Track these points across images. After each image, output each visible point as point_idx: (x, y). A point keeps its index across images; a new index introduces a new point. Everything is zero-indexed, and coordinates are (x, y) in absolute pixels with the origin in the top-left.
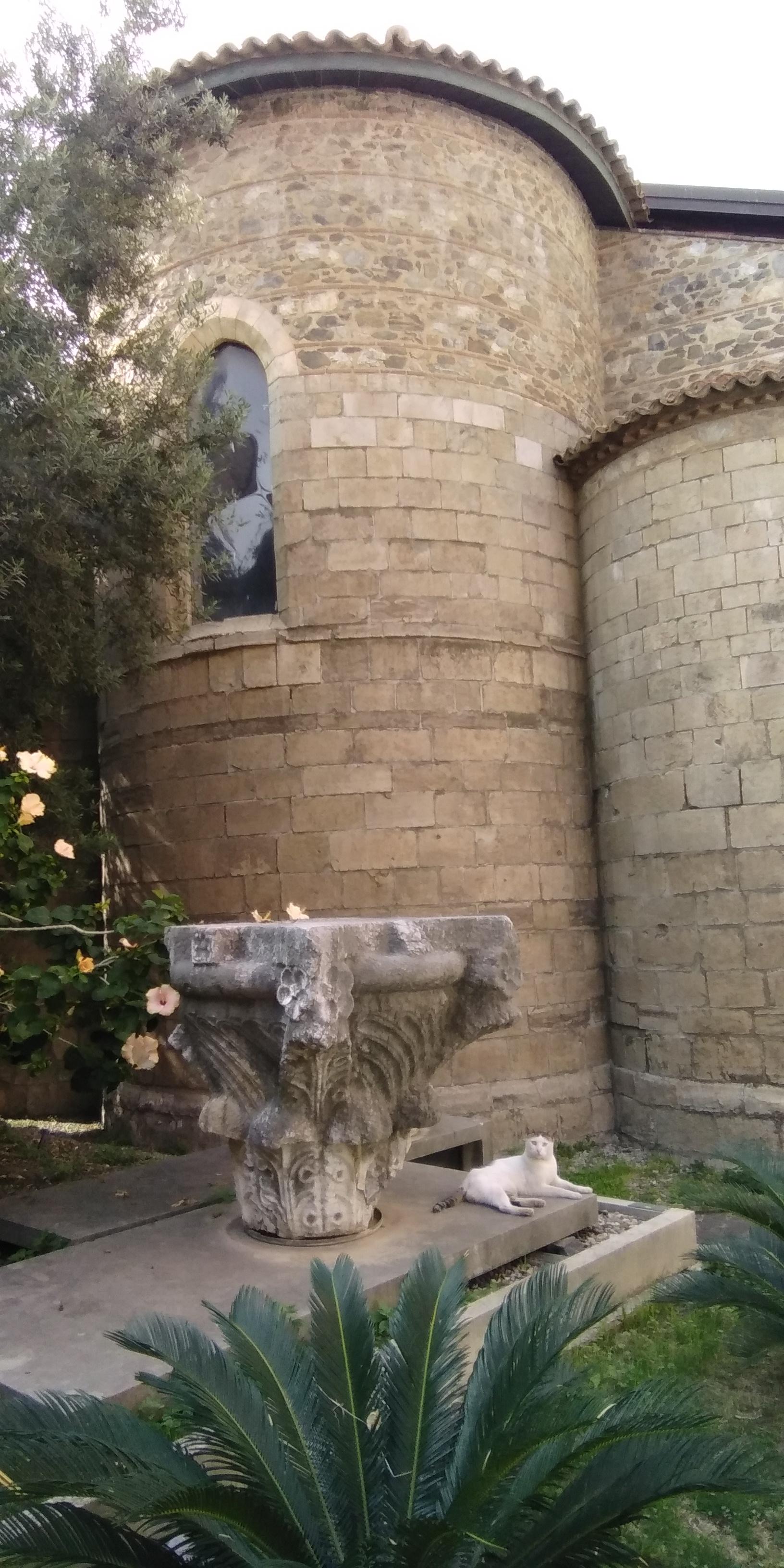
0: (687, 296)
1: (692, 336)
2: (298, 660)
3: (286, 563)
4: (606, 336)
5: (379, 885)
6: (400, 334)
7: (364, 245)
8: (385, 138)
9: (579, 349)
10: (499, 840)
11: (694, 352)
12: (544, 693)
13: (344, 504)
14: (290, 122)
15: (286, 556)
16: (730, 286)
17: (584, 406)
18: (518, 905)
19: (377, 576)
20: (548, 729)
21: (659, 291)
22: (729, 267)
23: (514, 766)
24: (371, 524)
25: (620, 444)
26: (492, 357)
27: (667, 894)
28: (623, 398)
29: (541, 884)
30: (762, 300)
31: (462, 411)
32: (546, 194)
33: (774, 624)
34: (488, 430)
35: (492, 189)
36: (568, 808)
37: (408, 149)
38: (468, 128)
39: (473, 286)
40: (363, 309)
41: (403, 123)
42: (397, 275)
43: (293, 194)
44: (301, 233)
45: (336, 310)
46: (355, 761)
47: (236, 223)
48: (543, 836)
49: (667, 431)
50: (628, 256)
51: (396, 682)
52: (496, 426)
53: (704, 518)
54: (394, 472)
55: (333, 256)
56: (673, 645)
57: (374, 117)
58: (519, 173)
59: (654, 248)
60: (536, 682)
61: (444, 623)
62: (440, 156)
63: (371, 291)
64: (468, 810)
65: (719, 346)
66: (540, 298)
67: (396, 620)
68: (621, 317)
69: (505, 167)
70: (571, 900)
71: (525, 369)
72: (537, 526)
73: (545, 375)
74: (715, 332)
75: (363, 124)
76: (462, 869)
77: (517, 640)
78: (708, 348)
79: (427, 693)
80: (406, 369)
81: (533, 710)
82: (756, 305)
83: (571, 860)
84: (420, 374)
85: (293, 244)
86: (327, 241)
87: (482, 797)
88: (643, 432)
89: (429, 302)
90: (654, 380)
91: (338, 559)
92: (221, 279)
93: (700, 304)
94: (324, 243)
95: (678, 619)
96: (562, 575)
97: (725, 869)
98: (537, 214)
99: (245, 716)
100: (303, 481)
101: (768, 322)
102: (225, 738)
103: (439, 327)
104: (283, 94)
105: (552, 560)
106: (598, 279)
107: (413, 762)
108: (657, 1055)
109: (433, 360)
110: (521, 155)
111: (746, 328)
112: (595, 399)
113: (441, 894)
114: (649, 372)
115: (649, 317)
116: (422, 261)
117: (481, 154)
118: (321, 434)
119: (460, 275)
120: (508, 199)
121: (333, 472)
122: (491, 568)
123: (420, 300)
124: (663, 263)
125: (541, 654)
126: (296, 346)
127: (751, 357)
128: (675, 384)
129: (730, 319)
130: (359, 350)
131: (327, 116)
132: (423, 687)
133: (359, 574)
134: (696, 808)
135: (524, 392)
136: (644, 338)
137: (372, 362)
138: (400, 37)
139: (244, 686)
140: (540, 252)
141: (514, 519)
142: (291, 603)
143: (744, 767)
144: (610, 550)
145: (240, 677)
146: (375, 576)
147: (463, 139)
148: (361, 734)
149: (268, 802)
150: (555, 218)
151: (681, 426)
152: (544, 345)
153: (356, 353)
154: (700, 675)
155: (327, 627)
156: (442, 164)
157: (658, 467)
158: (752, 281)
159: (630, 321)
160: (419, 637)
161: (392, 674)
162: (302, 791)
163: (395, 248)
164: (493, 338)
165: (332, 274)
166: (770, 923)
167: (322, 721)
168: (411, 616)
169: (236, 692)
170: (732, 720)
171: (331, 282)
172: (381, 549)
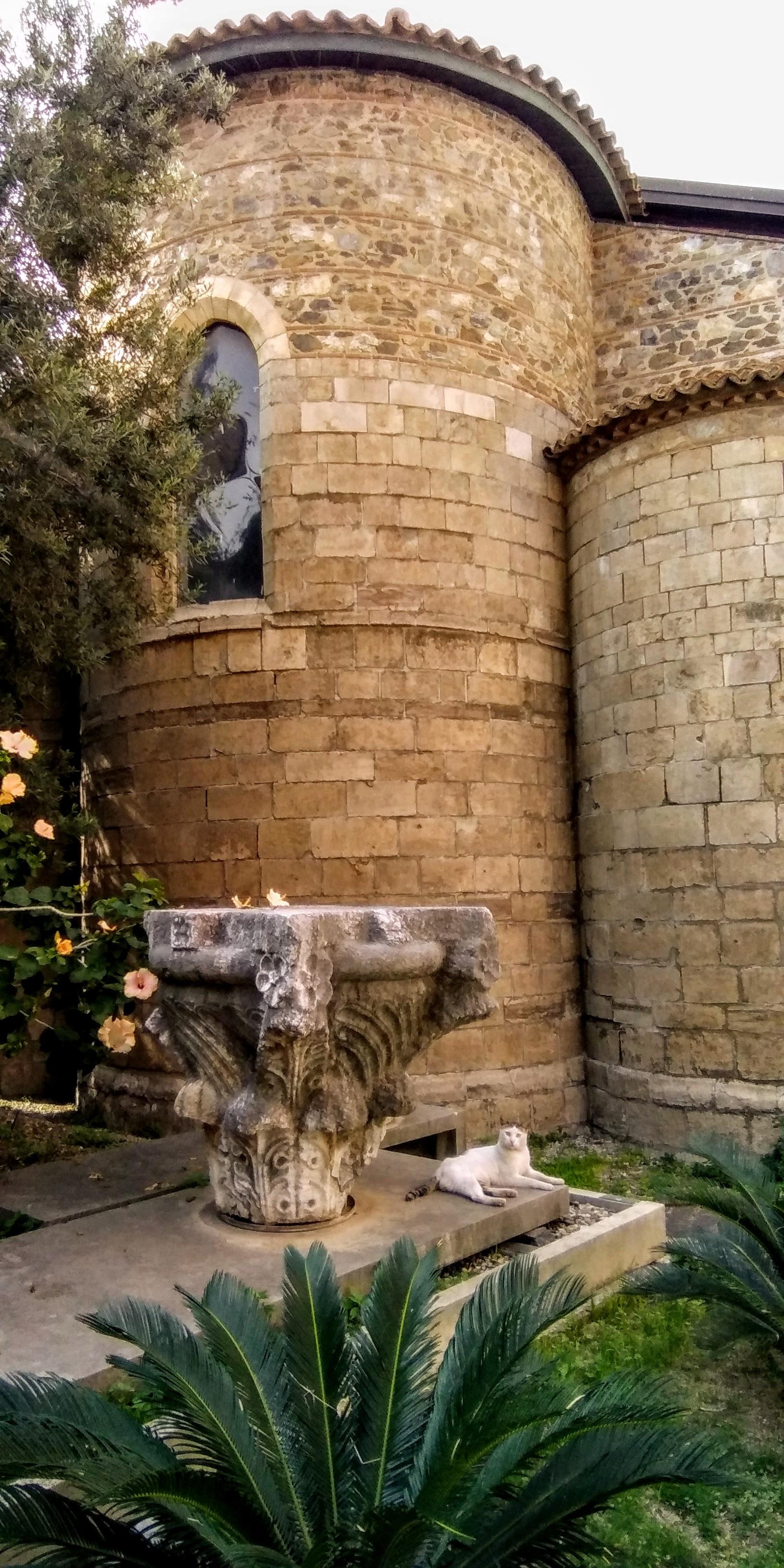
0: (680, 291)
3: (274, 548)
4: (599, 328)
5: (359, 873)
6: (393, 320)
10: (479, 831)
11: (686, 348)
12: (528, 685)
13: (333, 490)
14: (287, 102)
16: (724, 283)
17: (576, 399)
23: (496, 758)
24: (359, 510)
28: (613, 392)
31: (453, 400)
33: (757, 623)
34: (478, 420)
36: (549, 801)
38: (467, 115)
39: (467, 274)
41: (401, 107)
42: (391, 261)
43: (288, 175)
44: (297, 214)
46: (338, 748)
47: (230, 202)
50: (622, 249)
51: (381, 671)
52: (487, 416)
53: (690, 515)
54: (384, 458)
55: (328, 239)
56: (657, 641)
59: (648, 243)
60: (521, 674)
61: (430, 612)
62: (437, 142)
63: (364, 275)
64: (450, 801)
65: (710, 343)
66: (534, 289)
67: (383, 608)
70: (550, 893)
71: (516, 359)
72: (525, 518)
73: (537, 366)
74: (706, 329)
75: (361, 106)
79: (412, 682)
80: (398, 355)
81: (517, 702)
83: (550, 852)
84: (412, 361)
85: (287, 226)
87: (464, 788)
89: (422, 289)
91: (328, 544)
92: (214, 258)
93: (693, 300)
96: (548, 567)
97: (703, 865)
98: (533, 204)
101: (760, 320)
103: (433, 314)
105: (540, 552)
106: (591, 270)
108: (630, 1047)
109: (426, 347)
113: (421, 883)
115: (642, 311)
116: (417, 247)
119: (455, 263)
122: (479, 558)
123: (413, 286)
125: (526, 646)
128: (666, 380)
129: (722, 316)
130: (351, 335)
131: (324, 97)
133: (347, 561)
135: (516, 383)
136: (636, 333)
138: (400, 20)
140: (535, 242)
142: (278, 588)
143: (725, 765)
144: (597, 543)
148: (345, 722)
149: (250, 788)
150: (551, 208)
151: (672, 422)
154: (683, 672)
155: (313, 613)
156: (439, 150)
158: (745, 279)
159: (623, 315)
161: (377, 662)
165: (326, 257)
167: (306, 708)
169: (220, 676)
170: (713, 717)
171: (325, 265)
172: (369, 536)
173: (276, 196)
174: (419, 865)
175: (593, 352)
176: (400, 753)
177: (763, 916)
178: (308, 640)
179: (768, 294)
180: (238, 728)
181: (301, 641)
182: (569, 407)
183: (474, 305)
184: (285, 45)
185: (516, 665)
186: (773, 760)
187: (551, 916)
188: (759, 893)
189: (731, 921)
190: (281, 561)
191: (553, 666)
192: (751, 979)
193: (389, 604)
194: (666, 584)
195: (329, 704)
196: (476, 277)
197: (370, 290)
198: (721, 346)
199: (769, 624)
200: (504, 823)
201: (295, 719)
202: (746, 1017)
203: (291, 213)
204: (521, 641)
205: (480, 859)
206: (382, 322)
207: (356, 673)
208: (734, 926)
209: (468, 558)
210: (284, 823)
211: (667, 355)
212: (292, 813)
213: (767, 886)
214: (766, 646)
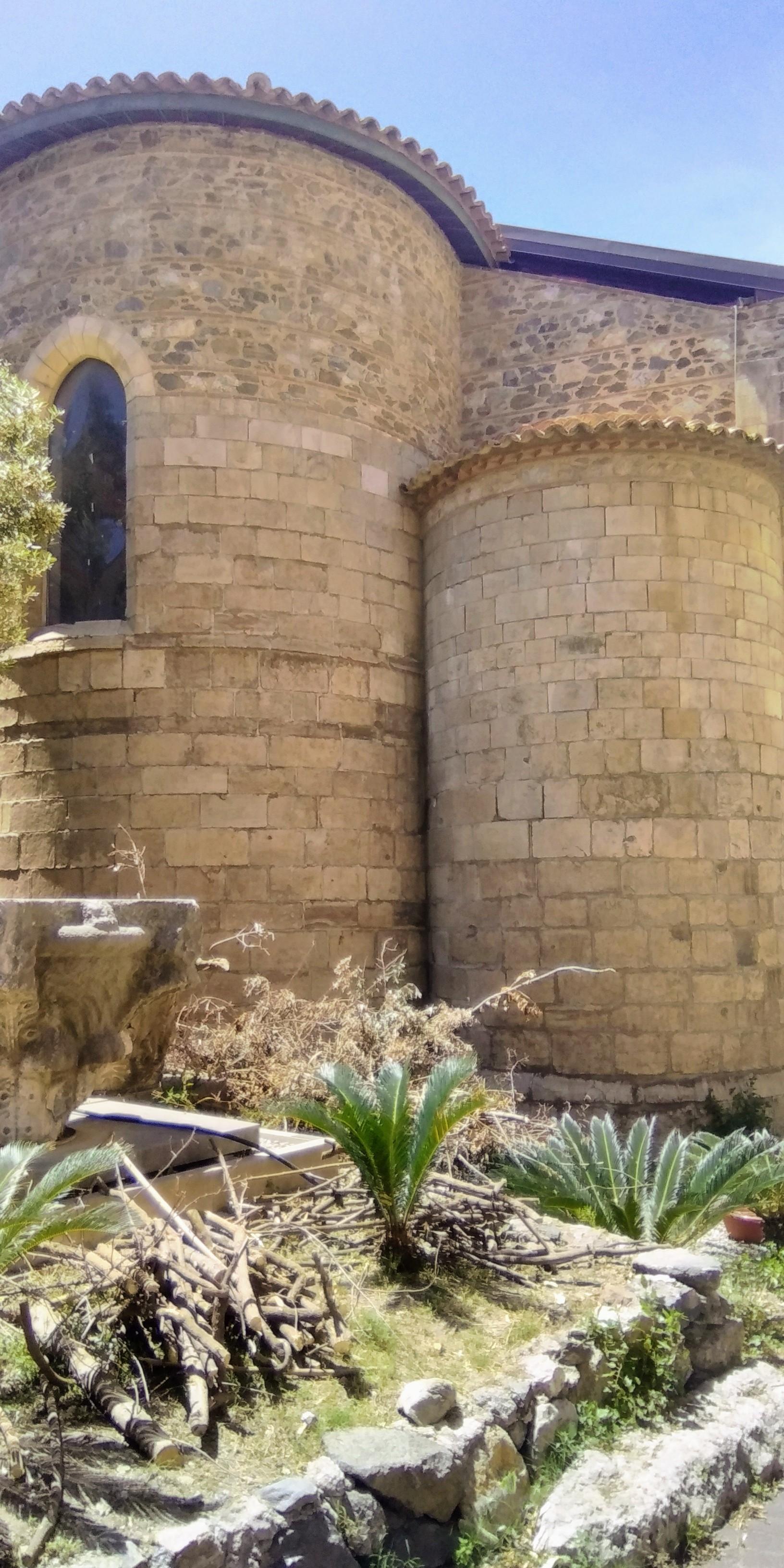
0: (540, 336)
1: (543, 375)
3: (135, 573)
4: (466, 368)
5: (211, 881)
6: (254, 362)
7: (223, 276)
9: (434, 382)
11: (544, 390)
12: (380, 707)
13: (193, 520)
14: (156, 154)
17: (437, 437)
19: (220, 591)
23: (346, 774)
25: (456, 478)
26: (342, 388)
27: (478, 897)
28: (478, 429)
31: (309, 438)
33: (577, 655)
34: (335, 458)
35: (349, 228)
36: (398, 817)
38: (329, 171)
41: (266, 162)
42: (253, 307)
43: (157, 223)
49: (496, 470)
50: (489, 294)
51: (236, 691)
52: (343, 454)
53: (523, 553)
54: (243, 492)
55: (194, 286)
56: (493, 669)
57: (238, 155)
58: (378, 214)
59: (512, 289)
60: (373, 696)
61: (285, 637)
62: (299, 196)
64: (300, 814)
65: (566, 386)
66: (394, 335)
68: (479, 352)
71: (374, 400)
72: (379, 550)
75: (227, 161)
76: (292, 869)
77: (355, 655)
78: (555, 387)
80: (258, 395)
83: (399, 863)
84: (271, 401)
85: (154, 271)
86: (187, 270)
88: (475, 469)
89: (283, 334)
91: (191, 569)
93: (551, 345)
95: (498, 646)
96: (403, 598)
98: (395, 254)
99: (90, 715)
101: (610, 367)
102: (70, 735)
103: (292, 359)
106: (460, 313)
107: (248, 766)
109: (285, 388)
110: (381, 197)
112: (449, 429)
116: (279, 294)
117: (341, 195)
118: (174, 452)
119: (315, 309)
122: (332, 587)
126: (153, 368)
129: (577, 361)
130: (213, 375)
131: (193, 151)
133: (205, 587)
135: (373, 422)
136: (499, 374)
138: (261, 84)
140: (396, 290)
142: (139, 611)
143: (548, 784)
145: (86, 678)
147: (323, 181)
148: (201, 738)
149: (109, 799)
150: (414, 257)
151: (507, 467)
152: (396, 377)
155: (173, 635)
156: (302, 204)
159: (488, 356)
163: (252, 281)
165: (191, 302)
166: (559, 928)
167: (163, 724)
170: (537, 741)
172: (225, 563)
173: (145, 242)
174: (269, 874)
176: (255, 768)
177: (577, 924)
178: (167, 661)
179: (619, 342)
180: (99, 741)
181: (158, 660)
182: (428, 445)
184: (152, 104)
186: (589, 780)
187: (397, 923)
188: (574, 902)
191: (406, 689)
193: (245, 629)
194: (501, 617)
195: (185, 720)
196: (335, 323)
197: (232, 334)
198: (575, 389)
199: (588, 655)
200: (353, 835)
201: (153, 735)
202: (561, 1016)
203: (159, 259)
204: (374, 665)
205: (328, 869)
206: (243, 364)
207: (212, 693)
208: (553, 932)
210: (141, 833)
211: (525, 396)
212: (147, 824)
213: (582, 895)
214: (585, 676)
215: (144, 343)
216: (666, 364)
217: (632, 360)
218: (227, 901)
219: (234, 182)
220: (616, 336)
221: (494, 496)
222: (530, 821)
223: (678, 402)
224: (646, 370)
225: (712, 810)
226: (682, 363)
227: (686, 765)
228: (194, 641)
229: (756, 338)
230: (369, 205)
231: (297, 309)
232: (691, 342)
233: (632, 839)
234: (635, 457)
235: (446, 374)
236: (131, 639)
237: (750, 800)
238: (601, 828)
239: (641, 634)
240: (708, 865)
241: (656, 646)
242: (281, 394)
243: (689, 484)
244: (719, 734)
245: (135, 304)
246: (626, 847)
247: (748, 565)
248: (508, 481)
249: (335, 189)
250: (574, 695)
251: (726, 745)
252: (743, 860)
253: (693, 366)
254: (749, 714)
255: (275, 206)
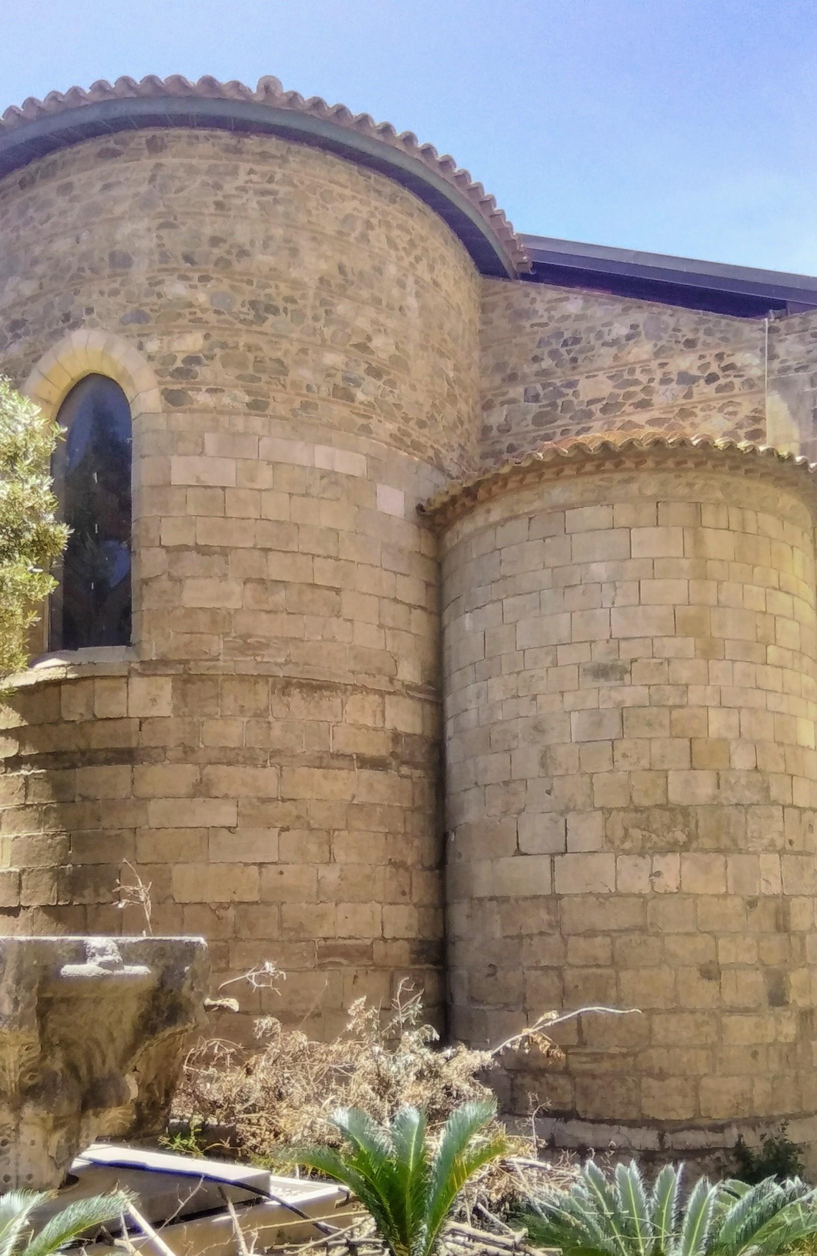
0: (563, 350)
1: (566, 391)
2: (149, 694)
3: (141, 597)
4: (485, 384)
6: (264, 377)
7: (232, 287)
8: (257, 183)
9: (452, 398)
12: (396, 737)
13: (201, 542)
14: (163, 161)
15: (141, 589)
16: (603, 345)
17: (455, 455)
18: (359, 942)
19: (230, 615)
20: (398, 771)
21: (536, 344)
22: (603, 325)
23: (361, 807)
24: (227, 563)
26: (356, 404)
28: (498, 447)
29: (382, 922)
30: (632, 361)
31: (323, 457)
32: (422, 244)
33: (602, 682)
34: (349, 477)
35: (364, 238)
36: (415, 851)
37: (280, 195)
38: (343, 178)
39: (340, 334)
40: (228, 351)
41: (277, 169)
42: (264, 320)
43: (164, 232)
45: (200, 351)
48: (388, 876)
50: (509, 306)
51: (246, 720)
52: (357, 473)
53: (545, 577)
54: (253, 513)
55: (202, 298)
56: (513, 697)
57: (248, 161)
59: (533, 301)
60: (388, 726)
61: (297, 664)
62: (312, 204)
64: (313, 848)
65: (590, 402)
66: (411, 349)
67: (249, 659)
68: (500, 367)
69: (379, 217)
70: (414, 940)
71: (390, 416)
72: (395, 573)
73: (412, 423)
75: (236, 168)
76: (304, 905)
77: (370, 683)
79: (277, 730)
80: (269, 412)
82: (626, 365)
83: (415, 899)
84: (282, 418)
85: (160, 282)
86: (195, 282)
88: (495, 489)
89: (294, 348)
90: (527, 432)
91: (199, 593)
93: (574, 360)
94: (192, 283)
95: (518, 673)
96: (420, 623)
97: (548, 913)
98: (411, 264)
100: (161, 517)
101: (636, 382)
102: (73, 766)
103: (304, 374)
104: (159, 132)
105: (410, 606)
106: (479, 326)
109: (297, 405)
110: (397, 206)
111: (615, 387)
112: (468, 447)
113: (281, 927)
114: (524, 423)
116: (290, 307)
117: (355, 203)
118: (181, 471)
119: (328, 322)
120: (380, 249)
121: (191, 510)
122: (346, 612)
124: (542, 316)
125: (394, 698)
126: (160, 383)
127: (619, 416)
129: (602, 376)
130: (222, 391)
131: (201, 157)
132: (272, 725)
133: (214, 611)
134: (526, 854)
135: (389, 440)
136: (520, 390)
137: (235, 404)
138: (272, 87)
139: (94, 716)
140: (412, 302)
141: (372, 565)
142: (145, 636)
143: (570, 817)
144: (463, 600)
145: (90, 707)
146: (229, 614)
147: (337, 189)
148: (209, 769)
149: (113, 832)
150: (432, 268)
151: (529, 487)
152: (413, 393)
153: (219, 394)
155: (180, 662)
156: (314, 212)
157: (508, 524)
159: (509, 371)
160: (270, 676)
162: (147, 823)
163: (263, 293)
164: (359, 385)
165: (199, 315)
166: (583, 967)
167: (170, 754)
168: (263, 656)
169: (86, 721)
170: (560, 772)
172: (234, 586)
174: (280, 911)
175: (479, 406)
177: (601, 962)
179: (645, 357)
180: (104, 772)
181: (165, 688)
182: (446, 464)
183: (347, 365)
184: (158, 108)
185: (383, 716)
186: (614, 813)
187: (414, 962)
188: (599, 940)
189: (572, 966)
190: (149, 610)
191: (423, 718)
192: (589, 1023)
193: (255, 655)
194: (522, 643)
195: (193, 751)
196: (349, 336)
197: (241, 349)
198: (600, 406)
199: (613, 683)
200: (367, 870)
201: (159, 766)
203: (166, 270)
204: (390, 693)
207: (221, 722)
208: (576, 972)
209: (337, 613)
210: (146, 868)
211: (547, 413)
212: (153, 858)
213: (606, 933)
214: (610, 705)
215: (150, 358)
216: (694, 380)
217: (658, 375)
218: (237, 939)
219: (243, 189)
220: (642, 350)
221: (515, 517)
222: (552, 855)
223: (706, 418)
224: (674, 385)
225: (742, 844)
226: (711, 379)
227: (715, 797)
228: (202, 668)
229: (788, 353)
230: (385, 213)
231: (309, 322)
232: (720, 357)
233: (658, 874)
234: (662, 476)
235: (465, 390)
236: (136, 666)
237: (782, 834)
238: (626, 862)
239: (668, 660)
240: (738, 901)
241: (684, 673)
242: (294, 412)
243: (718, 504)
244: (750, 765)
245: (140, 317)
246: (652, 883)
247: (780, 589)
248: (529, 501)
249: (348, 196)
250: (599, 724)
251: (757, 777)
252: (775, 896)
253: (722, 381)
254: (781, 744)
255: (287, 215)
